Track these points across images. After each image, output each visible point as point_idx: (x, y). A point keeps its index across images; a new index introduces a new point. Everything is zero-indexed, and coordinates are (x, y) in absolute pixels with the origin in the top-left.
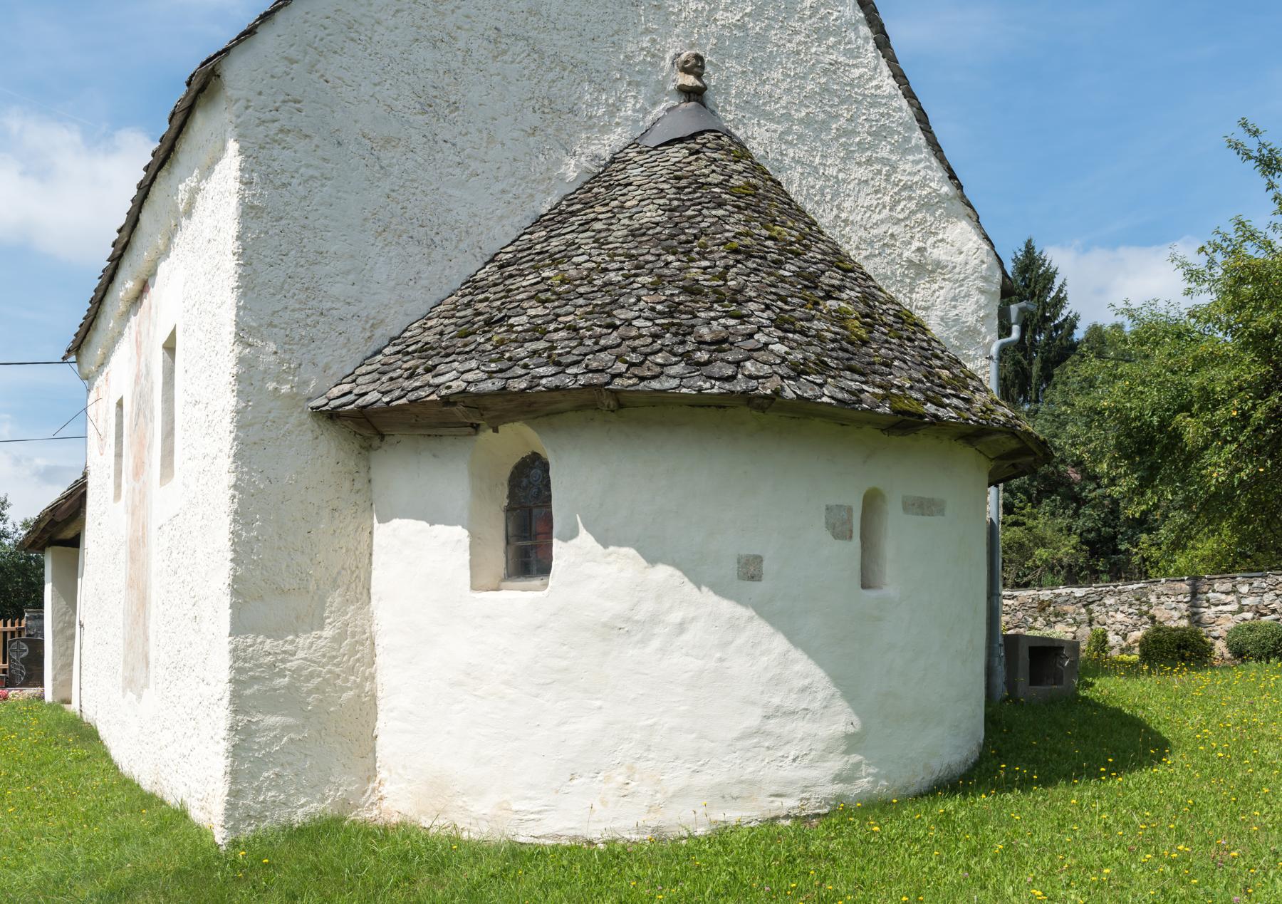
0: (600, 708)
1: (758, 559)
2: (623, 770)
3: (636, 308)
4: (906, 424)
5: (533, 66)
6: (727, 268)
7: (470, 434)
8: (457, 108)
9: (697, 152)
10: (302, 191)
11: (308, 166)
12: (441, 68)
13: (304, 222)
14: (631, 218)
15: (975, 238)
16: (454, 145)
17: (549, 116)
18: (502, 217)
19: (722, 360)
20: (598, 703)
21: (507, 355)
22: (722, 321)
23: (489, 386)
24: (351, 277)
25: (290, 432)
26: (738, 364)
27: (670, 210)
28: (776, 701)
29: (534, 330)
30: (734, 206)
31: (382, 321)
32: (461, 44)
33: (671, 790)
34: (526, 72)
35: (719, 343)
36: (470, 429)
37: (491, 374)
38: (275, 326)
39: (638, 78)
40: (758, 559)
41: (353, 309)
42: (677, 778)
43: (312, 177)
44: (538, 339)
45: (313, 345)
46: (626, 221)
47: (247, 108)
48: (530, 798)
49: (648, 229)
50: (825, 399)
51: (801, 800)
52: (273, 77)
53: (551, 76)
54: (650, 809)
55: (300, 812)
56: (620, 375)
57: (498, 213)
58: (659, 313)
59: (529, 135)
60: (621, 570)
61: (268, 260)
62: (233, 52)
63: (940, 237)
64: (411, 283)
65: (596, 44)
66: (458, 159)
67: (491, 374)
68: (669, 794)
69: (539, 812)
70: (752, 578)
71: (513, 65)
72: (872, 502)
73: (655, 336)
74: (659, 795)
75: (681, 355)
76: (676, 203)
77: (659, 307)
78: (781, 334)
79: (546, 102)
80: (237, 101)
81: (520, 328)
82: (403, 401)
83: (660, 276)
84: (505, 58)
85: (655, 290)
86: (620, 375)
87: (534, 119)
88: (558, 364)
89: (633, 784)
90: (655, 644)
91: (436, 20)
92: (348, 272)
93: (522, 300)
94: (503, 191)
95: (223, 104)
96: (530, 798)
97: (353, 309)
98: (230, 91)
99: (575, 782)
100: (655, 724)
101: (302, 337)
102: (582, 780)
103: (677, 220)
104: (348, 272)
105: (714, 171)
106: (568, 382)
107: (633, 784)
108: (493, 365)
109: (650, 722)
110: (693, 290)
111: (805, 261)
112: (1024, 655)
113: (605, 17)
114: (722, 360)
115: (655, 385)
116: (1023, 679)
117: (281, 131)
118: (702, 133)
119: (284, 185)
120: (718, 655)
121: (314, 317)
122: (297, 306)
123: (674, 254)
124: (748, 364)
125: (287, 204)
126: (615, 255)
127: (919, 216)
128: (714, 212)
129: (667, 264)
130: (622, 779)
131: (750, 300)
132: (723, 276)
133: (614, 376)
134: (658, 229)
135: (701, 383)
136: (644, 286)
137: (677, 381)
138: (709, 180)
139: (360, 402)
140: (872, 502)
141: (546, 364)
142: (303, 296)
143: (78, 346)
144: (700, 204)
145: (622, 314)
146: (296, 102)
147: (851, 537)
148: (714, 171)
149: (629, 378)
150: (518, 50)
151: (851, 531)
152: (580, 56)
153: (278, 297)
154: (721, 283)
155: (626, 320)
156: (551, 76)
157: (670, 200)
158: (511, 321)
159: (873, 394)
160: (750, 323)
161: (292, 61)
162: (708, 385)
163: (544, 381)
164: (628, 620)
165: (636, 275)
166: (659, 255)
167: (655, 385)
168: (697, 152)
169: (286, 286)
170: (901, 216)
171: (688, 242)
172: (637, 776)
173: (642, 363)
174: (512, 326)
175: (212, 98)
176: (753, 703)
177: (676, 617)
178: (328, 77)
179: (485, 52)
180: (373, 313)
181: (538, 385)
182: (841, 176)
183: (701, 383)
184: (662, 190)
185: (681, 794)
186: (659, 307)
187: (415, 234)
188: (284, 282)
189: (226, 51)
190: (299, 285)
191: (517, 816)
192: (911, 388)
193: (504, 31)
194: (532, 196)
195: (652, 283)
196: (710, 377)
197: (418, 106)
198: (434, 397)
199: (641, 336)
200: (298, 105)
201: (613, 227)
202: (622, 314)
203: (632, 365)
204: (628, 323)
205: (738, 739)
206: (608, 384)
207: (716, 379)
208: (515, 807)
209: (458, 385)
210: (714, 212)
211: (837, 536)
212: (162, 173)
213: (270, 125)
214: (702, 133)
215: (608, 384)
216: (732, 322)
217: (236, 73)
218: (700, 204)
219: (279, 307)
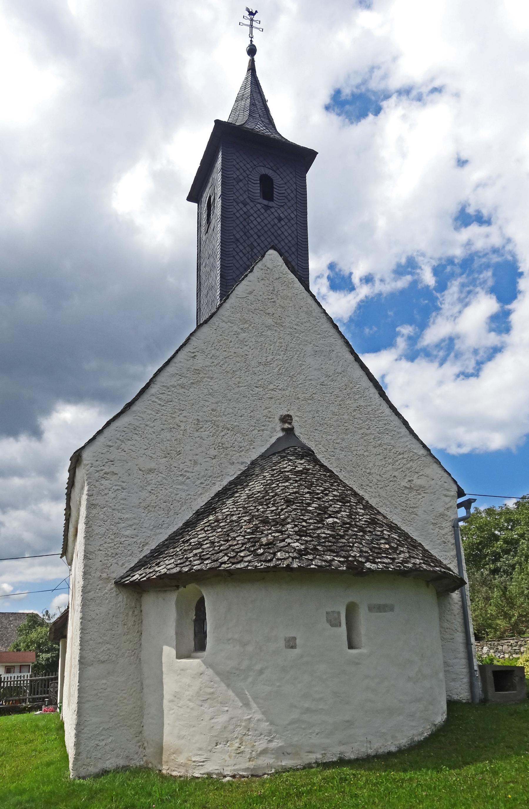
0: (227, 711)
1: (295, 638)
2: (238, 740)
3: (239, 531)
4: (356, 572)
5: (214, 431)
6: (282, 510)
7: (176, 590)
8: (180, 453)
9: (285, 457)
10: (113, 495)
11: (116, 485)
12: (173, 439)
13: (114, 507)
14: (250, 490)
15: (440, 472)
16: (179, 468)
17: (221, 450)
18: (201, 494)
19: (268, 552)
20: (226, 709)
21: (185, 556)
22: (273, 534)
23: (175, 571)
24: (133, 527)
25: (107, 593)
26: (275, 554)
27: (266, 485)
28: (306, 705)
29: (198, 544)
30: (294, 480)
31: (147, 543)
32: (182, 428)
33: (259, 750)
34: (211, 434)
35: (270, 544)
36: (175, 588)
37: (177, 565)
38: (101, 550)
39: (263, 428)
40: (295, 638)
41: (134, 540)
42: (261, 745)
43: (118, 489)
44: (199, 548)
45: (117, 556)
46: (247, 492)
47: (91, 467)
48: (199, 755)
49: (255, 495)
50: (312, 566)
51: (322, 754)
52: (102, 454)
53: (223, 433)
54: (250, 759)
55: (107, 762)
56: (225, 563)
57: (199, 493)
58: (248, 533)
59: (213, 459)
60: (234, 647)
61: (99, 524)
62: (86, 448)
63: (420, 474)
64: (160, 526)
65: (243, 418)
66: (181, 473)
67: (177, 565)
68: (258, 752)
69: (203, 762)
70: (292, 647)
71: (206, 432)
72: (351, 610)
73: (243, 544)
74: (254, 753)
75: (252, 551)
76: (269, 482)
77: (248, 530)
78: (298, 537)
79: (220, 445)
80: (87, 465)
81: (193, 544)
82: (145, 579)
83: (253, 516)
84: (202, 430)
85: (249, 522)
86: (225, 563)
87: (215, 452)
88: (202, 559)
89: (242, 747)
90: (250, 679)
91: (171, 421)
92: (133, 525)
93: (198, 531)
94: (201, 483)
95: (82, 466)
96: (199, 755)
97: (134, 540)
98: (85, 462)
99: (218, 746)
100: (251, 718)
101: (112, 553)
102: (221, 745)
103: (267, 489)
104: (133, 525)
105: (289, 465)
106: (204, 567)
107: (242, 747)
108: (179, 561)
109: (249, 717)
110: (265, 522)
111: (323, 501)
112: (490, 675)
113: (247, 406)
114: (268, 552)
115: (239, 566)
116: (491, 689)
117: (105, 473)
118: (288, 448)
119: (106, 494)
120: (278, 684)
121: (118, 545)
122: (111, 541)
123: (262, 505)
124: (279, 554)
125: (107, 501)
126: (239, 508)
127: (409, 465)
128: (283, 484)
129: (258, 510)
130: (237, 745)
131: (288, 523)
132: (279, 514)
133: (222, 563)
134: (259, 494)
135: (257, 564)
136: (245, 521)
137: (247, 564)
138: (286, 470)
139: (131, 580)
140: (351, 610)
141: (198, 560)
142: (113, 537)
143: (65, 552)
144: (279, 481)
145: (233, 535)
146: (112, 461)
147: (340, 626)
148: (289, 465)
149: (228, 564)
150: (207, 426)
151: (340, 623)
152: (235, 424)
153: (102, 539)
154: (278, 517)
155: (234, 537)
156: (223, 433)
157: (267, 480)
158: (191, 541)
159: (339, 561)
160: (285, 534)
161: (110, 446)
162: (260, 564)
163: (194, 568)
164: (237, 669)
165: (244, 517)
166: (255, 507)
167: (239, 566)
168: (285, 457)
169: (106, 534)
170: (399, 467)
171: (269, 499)
172: (244, 743)
173: (235, 556)
174: (191, 543)
175: (80, 464)
176: (296, 707)
177: (258, 667)
178: (125, 450)
179: (193, 429)
180: (143, 540)
181: (193, 569)
182: (366, 454)
183: (257, 564)
184: (265, 476)
185: (264, 752)
186: (248, 530)
187: (162, 506)
188: (105, 532)
189: (83, 448)
190: (111, 533)
191: (194, 764)
192: (360, 556)
193: (201, 420)
194: (214, 483)
195: (248, 520)
196: (261, 561)
197: (163, 455)
198: (154, 577)
199: (238, 544)
200: (112, 463)
201: (242, 495)
202: (233, 535)
203: (230, 558)
204: (234, 539)
205: (289, 724)
206: (219, 567)
207: (264, 561)
208: (194, 759)
209: (164, 571)
210: (283, 484)
211: (332, 625)
212: (72, 490)
213: (100, 472)
214: (288, 448)
215: (219, 567)
216: (277, 534)
217: (86, 455)
218: (279, 481)
219: (103, 542)
